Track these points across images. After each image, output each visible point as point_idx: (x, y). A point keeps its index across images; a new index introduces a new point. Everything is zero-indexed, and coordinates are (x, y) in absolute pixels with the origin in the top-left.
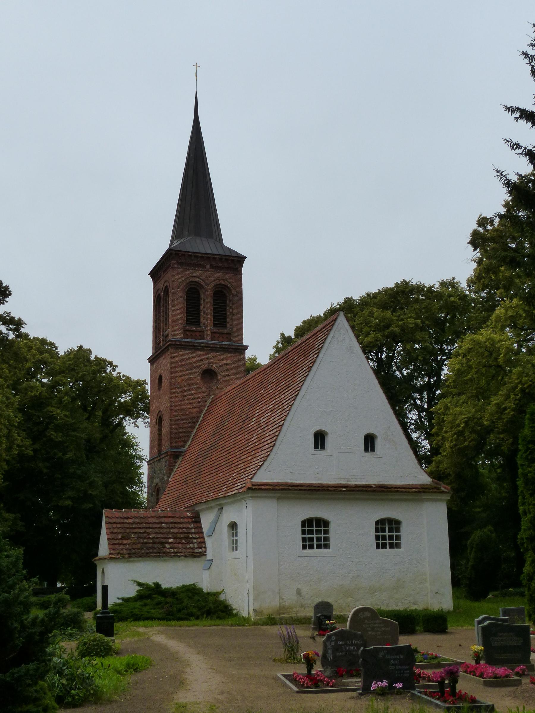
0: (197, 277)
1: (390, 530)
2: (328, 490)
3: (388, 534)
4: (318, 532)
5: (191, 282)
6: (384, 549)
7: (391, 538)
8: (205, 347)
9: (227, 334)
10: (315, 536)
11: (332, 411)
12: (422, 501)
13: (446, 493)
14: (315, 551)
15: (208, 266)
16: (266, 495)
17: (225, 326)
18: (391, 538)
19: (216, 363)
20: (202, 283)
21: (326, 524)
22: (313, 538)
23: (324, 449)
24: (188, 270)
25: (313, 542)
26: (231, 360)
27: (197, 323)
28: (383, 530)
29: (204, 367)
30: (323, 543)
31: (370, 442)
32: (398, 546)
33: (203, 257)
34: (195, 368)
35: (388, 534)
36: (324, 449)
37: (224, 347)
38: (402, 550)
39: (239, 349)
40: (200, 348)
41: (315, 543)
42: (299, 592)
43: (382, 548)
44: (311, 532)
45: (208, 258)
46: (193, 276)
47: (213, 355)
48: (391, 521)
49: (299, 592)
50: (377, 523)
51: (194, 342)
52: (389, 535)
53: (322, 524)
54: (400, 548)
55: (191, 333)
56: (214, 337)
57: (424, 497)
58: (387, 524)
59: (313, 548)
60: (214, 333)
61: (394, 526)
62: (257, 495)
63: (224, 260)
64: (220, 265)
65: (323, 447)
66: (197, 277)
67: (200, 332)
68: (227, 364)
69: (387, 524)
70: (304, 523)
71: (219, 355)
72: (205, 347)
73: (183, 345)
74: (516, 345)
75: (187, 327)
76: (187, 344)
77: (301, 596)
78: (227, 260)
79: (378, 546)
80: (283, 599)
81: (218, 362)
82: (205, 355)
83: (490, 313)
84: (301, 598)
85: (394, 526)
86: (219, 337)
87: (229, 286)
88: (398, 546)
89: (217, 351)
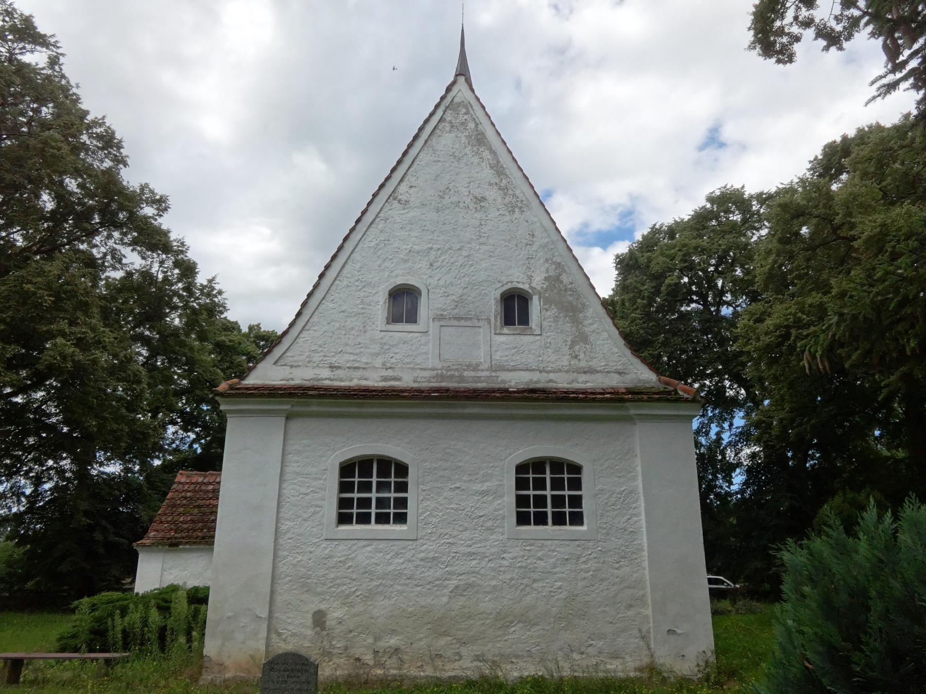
1: (557, 484)
2: (594, 400)
3: (549, 494)
4: (381, 487)
6: (541, 527)
7: (558, 501)
10: (548, 493)
11: (431, 248)
12: (630, 419)
13: (687, 400)
14: (550, 529)
18: (558, 501)
21: (402, 470)
22: (370, 499)
23: (415, 322)
25: (370, 508)
28: (540, 484)
30: (392, 511)
32: (577, 519)
35: (549, 494)
36: (415, 322)
38: (584, 528)
41: (373, 511)
42: (319, 619)
43: (536, 523)
44: (366, 487)
48: (386, 465)
49: (319, 619)
50: (521, 469)
53: (568, 473)
54: (582, 524)
57: (633, 412)
59: (369, 522)
61: (566, 476)
62: (681, 413)
65: (412, 318)
70: (346, 469)
77: (323, 629)
79: (522, 519)
80: (279, 634)
84: (325, 633)
85: (531, 476)
88: (577, 519)
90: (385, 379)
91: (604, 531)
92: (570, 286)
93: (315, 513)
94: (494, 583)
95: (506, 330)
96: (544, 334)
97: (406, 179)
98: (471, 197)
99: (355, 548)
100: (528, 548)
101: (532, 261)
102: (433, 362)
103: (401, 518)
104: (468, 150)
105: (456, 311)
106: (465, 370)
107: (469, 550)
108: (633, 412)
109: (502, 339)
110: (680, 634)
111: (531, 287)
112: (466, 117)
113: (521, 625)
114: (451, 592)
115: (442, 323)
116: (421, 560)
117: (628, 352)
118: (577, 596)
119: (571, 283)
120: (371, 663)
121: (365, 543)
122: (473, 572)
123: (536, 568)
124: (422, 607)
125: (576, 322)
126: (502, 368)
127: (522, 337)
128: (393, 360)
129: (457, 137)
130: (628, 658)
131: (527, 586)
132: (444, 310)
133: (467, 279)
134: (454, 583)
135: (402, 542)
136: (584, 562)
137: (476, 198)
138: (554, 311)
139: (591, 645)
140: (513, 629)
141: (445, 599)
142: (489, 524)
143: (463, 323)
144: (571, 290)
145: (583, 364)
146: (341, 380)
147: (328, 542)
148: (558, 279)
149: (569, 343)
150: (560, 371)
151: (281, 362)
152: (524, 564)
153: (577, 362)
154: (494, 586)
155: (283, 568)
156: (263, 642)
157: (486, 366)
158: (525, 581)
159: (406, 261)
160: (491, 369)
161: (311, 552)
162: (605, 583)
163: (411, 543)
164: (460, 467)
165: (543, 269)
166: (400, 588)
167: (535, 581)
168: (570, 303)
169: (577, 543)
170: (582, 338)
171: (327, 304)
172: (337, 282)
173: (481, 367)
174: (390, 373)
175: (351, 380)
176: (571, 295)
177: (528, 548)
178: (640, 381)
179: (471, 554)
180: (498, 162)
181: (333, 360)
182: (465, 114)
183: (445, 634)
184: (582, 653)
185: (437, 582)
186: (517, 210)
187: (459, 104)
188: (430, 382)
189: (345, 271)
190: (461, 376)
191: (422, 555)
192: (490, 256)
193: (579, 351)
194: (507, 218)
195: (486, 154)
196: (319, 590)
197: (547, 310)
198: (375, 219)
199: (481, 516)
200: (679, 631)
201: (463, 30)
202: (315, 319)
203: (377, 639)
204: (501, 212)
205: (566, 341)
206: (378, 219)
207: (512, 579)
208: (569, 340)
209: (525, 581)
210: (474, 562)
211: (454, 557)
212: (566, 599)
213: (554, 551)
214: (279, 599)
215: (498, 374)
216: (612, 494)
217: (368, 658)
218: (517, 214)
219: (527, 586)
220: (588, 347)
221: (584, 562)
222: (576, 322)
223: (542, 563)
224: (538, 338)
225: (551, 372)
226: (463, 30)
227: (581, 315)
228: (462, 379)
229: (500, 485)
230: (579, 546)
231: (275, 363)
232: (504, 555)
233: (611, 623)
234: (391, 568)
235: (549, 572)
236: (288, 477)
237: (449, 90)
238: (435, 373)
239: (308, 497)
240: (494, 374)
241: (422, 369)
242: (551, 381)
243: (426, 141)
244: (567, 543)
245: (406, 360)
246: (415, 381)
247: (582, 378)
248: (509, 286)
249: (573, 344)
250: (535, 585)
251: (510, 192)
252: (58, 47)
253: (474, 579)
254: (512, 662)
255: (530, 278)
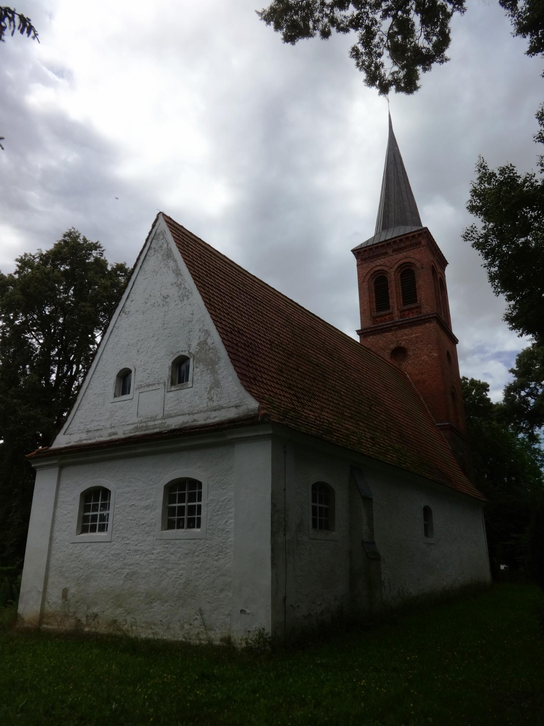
0: (380, 265)
3: (182, 505)
5: (376, 271)
8: (392, 327)
9: (417, 308)
11: (138, 340)
15: (390, 252)
16: (46, 463)
17: (416, 301)
19: (405, 340)
20: (386, 269)
24: (372, 262)
26: (421, 332)
27: (387, 306)
29: (393, 346)
31: (180, 370)
33: (384, 245)
34: (383, 349)
37: (410, 321)
39: (427, 318)
40: (388, 329)
45: (389, 244)
46: (378, 266)
47: (400, 333)
51: (379, 326)
52: (189, 506)
55: (381, 318)
56: (404, 315)
58: (175, 493)
60: (404, 311)
63: (404, 240)
64: (402, 245)
66: (380, 265)
67: (389, 314)
68: (417, 337)
69: (175, 493)
71: (406, 331)
72: (392, 327)
73: (370, 332)
74: (400, 37)
75: (375, 314)
76: (373, 329)
77: (66, 600)
78: (407, 238)
80: (49, 603)
81: (406, 337)
82: (393, 335)
83: (391, 31)
84: (67, 602)
86: (409, 314)
87: (413, 261)
89: (406, 328)
90: (110, 435)
91: (210, 532)
92: (211, 346)
93: (69, 526)
94: (146, 571)
95: (173, 388)
96: (195, 386)
97: (130, 297)
98: (161, 297)
99: (83, 548)
100: (166, 546)
101: (192, 333)
102: (136, 420)
103: (103, 528)
104: (162, 265)
105: (148, 381)
106: (149, 421)
107: (136, 548)
108: (229, 437)
109: (171, 394)
110: (249, 614)
111: (190, 353)
112: (163, 241)
113: (158, 602)
114: (125, 577)
115: (141, 390)
116: (112, 555)
117: (242, 389)
118: (191, 580)
119: (213, 343)
120: (85, 623)
121: (89, 544)
122: (137, 564)
123: (169, 560)
124: (111, 587)
125: (214, 372)
126: (170, 416)
127: (182, 391)
128: (115, 421)
129: (157, 257)
130: (218, 631)
131: (164, 573)
132: (142, 381)
133: (155, 356)
134: (126, 571)
135: (103, 544)
136: (197, 556)
137: (164, 297)
138: (201, 366)
139: (196, 619)
140: (154, 604)
141: (121, 582)
142: (147, 529)
143: (151, 388)
144: (212, 349)
145: (215, 404)
146: (90, 439)
147: (72, 545)
148: (205, 342)
149: (208, 389)
150: (201, 411)
151: (67, 433)
152: (163, 558)
153: (211, 403)
154: (146, 574)
155: (53, 561)
156: (39, 607)
157: (160, 416)
158: (163, 570)
159: (126, 352)
160: (163, 418)
161: (65, 551)
162: (208, 572)
163: (108, 544)
164: (136, 490)
165: (197, 337)
166: (101, 574)
167: (168, 570)
168: (211, 359)
169: (194, 541)
170: (216, 384)
171: (89, 391)
172: (94, 376)
173: (158, 417)
174: (113, 430)
175: (95, 438)
176: (212, 353)
177: (166, 546)
178: (249, 410)
179: (136, 551)
180: (177, 266)
181: (88, 427)
182: (162, 239)
183: (120, 606)
184: (191, 625)
185: (119, 571)
186: (185, 298)
187: (159, 234)
188: (131, 433)
189: (98, 367)
190: (147, 426)
191: (113, 552)
192: (169, 337)
193: (214, 394)
194: (179, 306)
195: (172, 264)
196: (66, 575)
197: (197, 368)
198: (113, 329)
199: (143, 524)
200: (248, 611)
201: (390, 116)
202: (83, 402)
203: (89, 608)
204: (177, 303)
205: (207, 388)
206: (115, 329)
207: (156, 568)
208: (208, 387)
209: (163, 570)
210: (138, 556)
211: (128, 553)
212: (185, 582)
213: (180, 547)
214: (50, 580)
215: (166, 420)
216: (218, 503)
217: (84, 620)
218: (185, 302)
219: (164, 573)
220: (219, 390)
221: (197, 556)
222: (214, 372)
223: (173, 557)
224: (191, 389)
225: (195, 413)
226: (390, 116)
227: (217, 366)
228: (147, 428)
229: (156, 501)
230: (195, 544)
231: (64, 434)
232: (153, 552)
233: (209, 602)
234: (98, 561)
235: (177, 563)
236: (59, 505)
237: (154, 226)
238: (133, 426)
239: (66, 517)
240: (164, 421)
241: (127, 425)
242: (195, 420)
243: (141, 267)
244: (188, 541)
245: (122, 420)
246: (124, 434)
247: (214, 414)
248: (178, 355)
249: (211, 388)
250: (168, 573)
251: (183, 286)
252: (101, 248)
253: (136, 568)
254: (152, 628)
255: (189, 346)
